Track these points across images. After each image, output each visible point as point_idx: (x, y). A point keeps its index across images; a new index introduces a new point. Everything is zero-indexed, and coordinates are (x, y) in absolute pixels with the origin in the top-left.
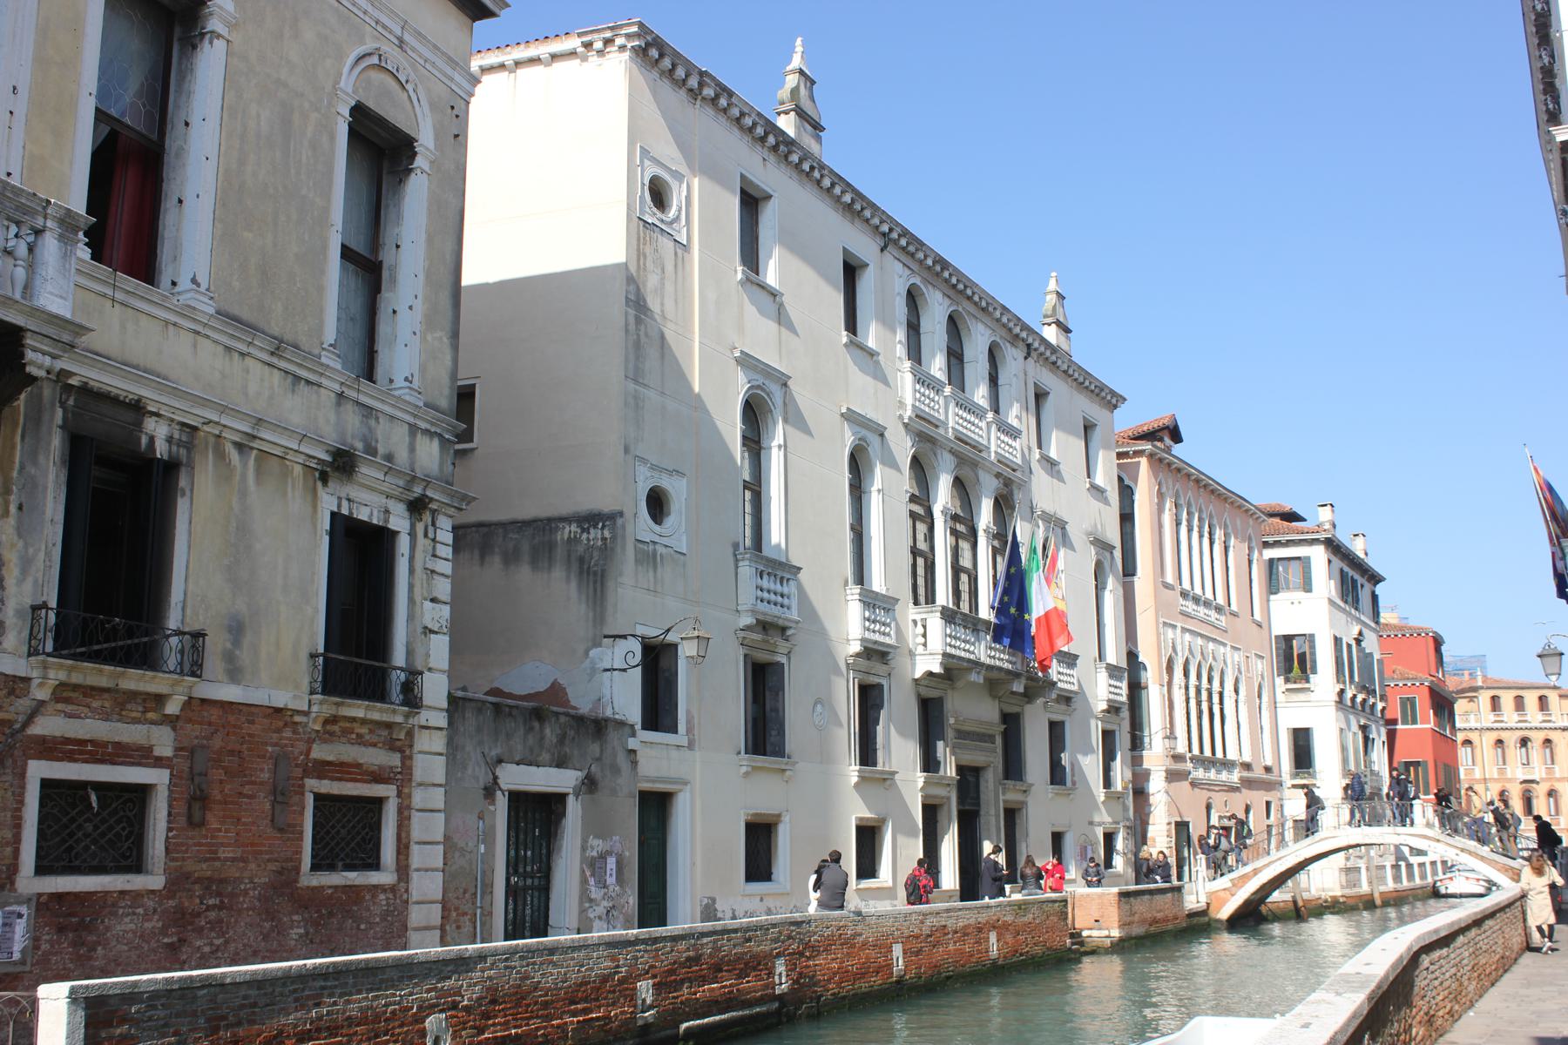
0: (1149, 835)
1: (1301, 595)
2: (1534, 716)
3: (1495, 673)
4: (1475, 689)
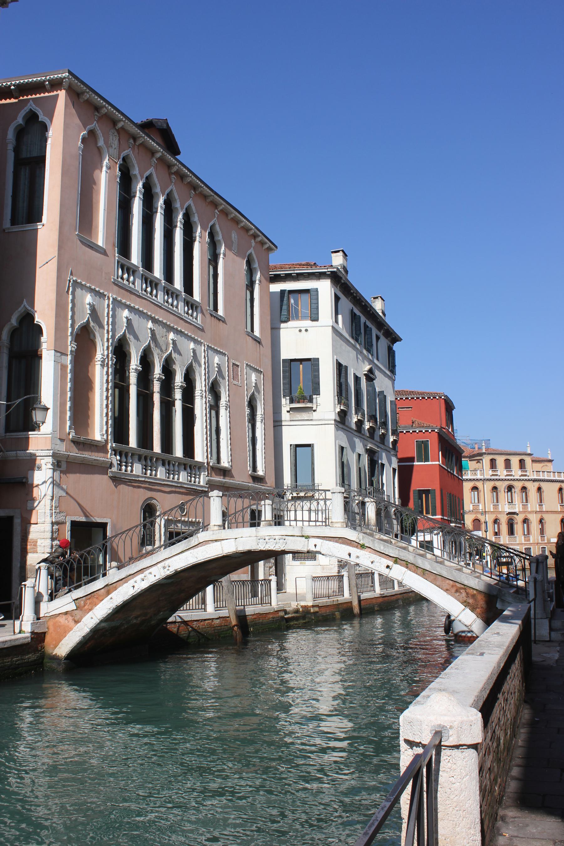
0: (31, 536)
1: (307, 323)
2: (516, 472)
3: (494, 446)
4: (481, 454)
